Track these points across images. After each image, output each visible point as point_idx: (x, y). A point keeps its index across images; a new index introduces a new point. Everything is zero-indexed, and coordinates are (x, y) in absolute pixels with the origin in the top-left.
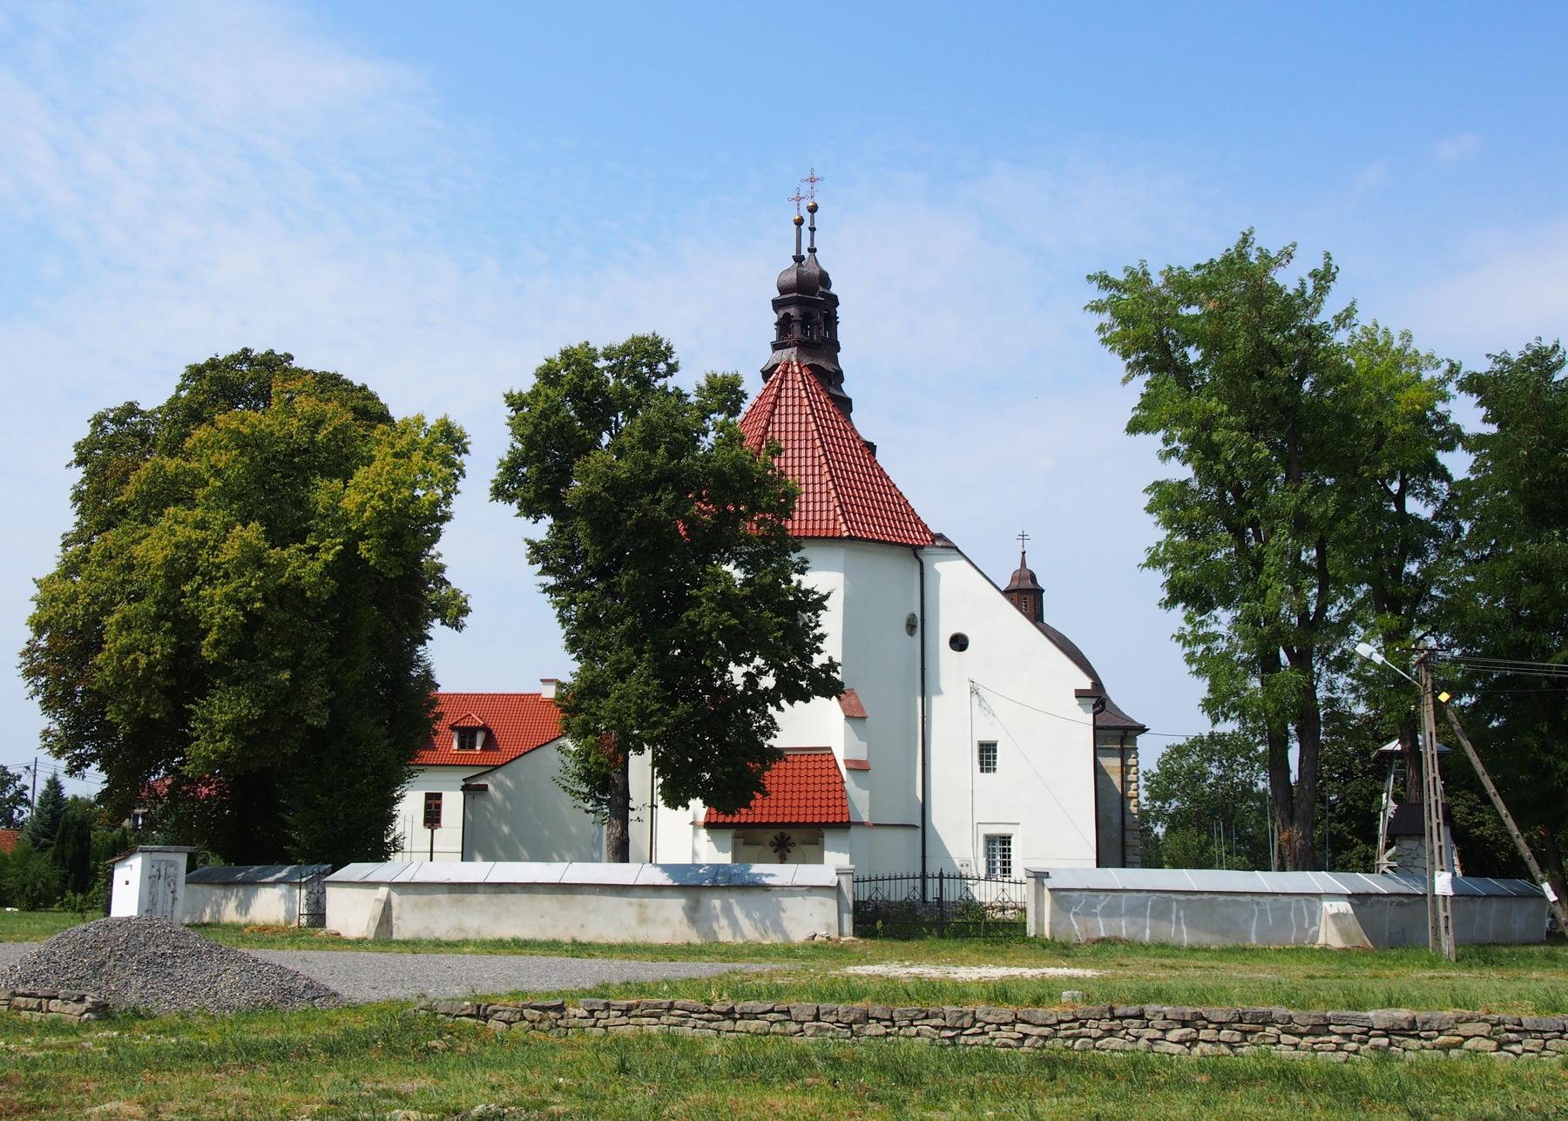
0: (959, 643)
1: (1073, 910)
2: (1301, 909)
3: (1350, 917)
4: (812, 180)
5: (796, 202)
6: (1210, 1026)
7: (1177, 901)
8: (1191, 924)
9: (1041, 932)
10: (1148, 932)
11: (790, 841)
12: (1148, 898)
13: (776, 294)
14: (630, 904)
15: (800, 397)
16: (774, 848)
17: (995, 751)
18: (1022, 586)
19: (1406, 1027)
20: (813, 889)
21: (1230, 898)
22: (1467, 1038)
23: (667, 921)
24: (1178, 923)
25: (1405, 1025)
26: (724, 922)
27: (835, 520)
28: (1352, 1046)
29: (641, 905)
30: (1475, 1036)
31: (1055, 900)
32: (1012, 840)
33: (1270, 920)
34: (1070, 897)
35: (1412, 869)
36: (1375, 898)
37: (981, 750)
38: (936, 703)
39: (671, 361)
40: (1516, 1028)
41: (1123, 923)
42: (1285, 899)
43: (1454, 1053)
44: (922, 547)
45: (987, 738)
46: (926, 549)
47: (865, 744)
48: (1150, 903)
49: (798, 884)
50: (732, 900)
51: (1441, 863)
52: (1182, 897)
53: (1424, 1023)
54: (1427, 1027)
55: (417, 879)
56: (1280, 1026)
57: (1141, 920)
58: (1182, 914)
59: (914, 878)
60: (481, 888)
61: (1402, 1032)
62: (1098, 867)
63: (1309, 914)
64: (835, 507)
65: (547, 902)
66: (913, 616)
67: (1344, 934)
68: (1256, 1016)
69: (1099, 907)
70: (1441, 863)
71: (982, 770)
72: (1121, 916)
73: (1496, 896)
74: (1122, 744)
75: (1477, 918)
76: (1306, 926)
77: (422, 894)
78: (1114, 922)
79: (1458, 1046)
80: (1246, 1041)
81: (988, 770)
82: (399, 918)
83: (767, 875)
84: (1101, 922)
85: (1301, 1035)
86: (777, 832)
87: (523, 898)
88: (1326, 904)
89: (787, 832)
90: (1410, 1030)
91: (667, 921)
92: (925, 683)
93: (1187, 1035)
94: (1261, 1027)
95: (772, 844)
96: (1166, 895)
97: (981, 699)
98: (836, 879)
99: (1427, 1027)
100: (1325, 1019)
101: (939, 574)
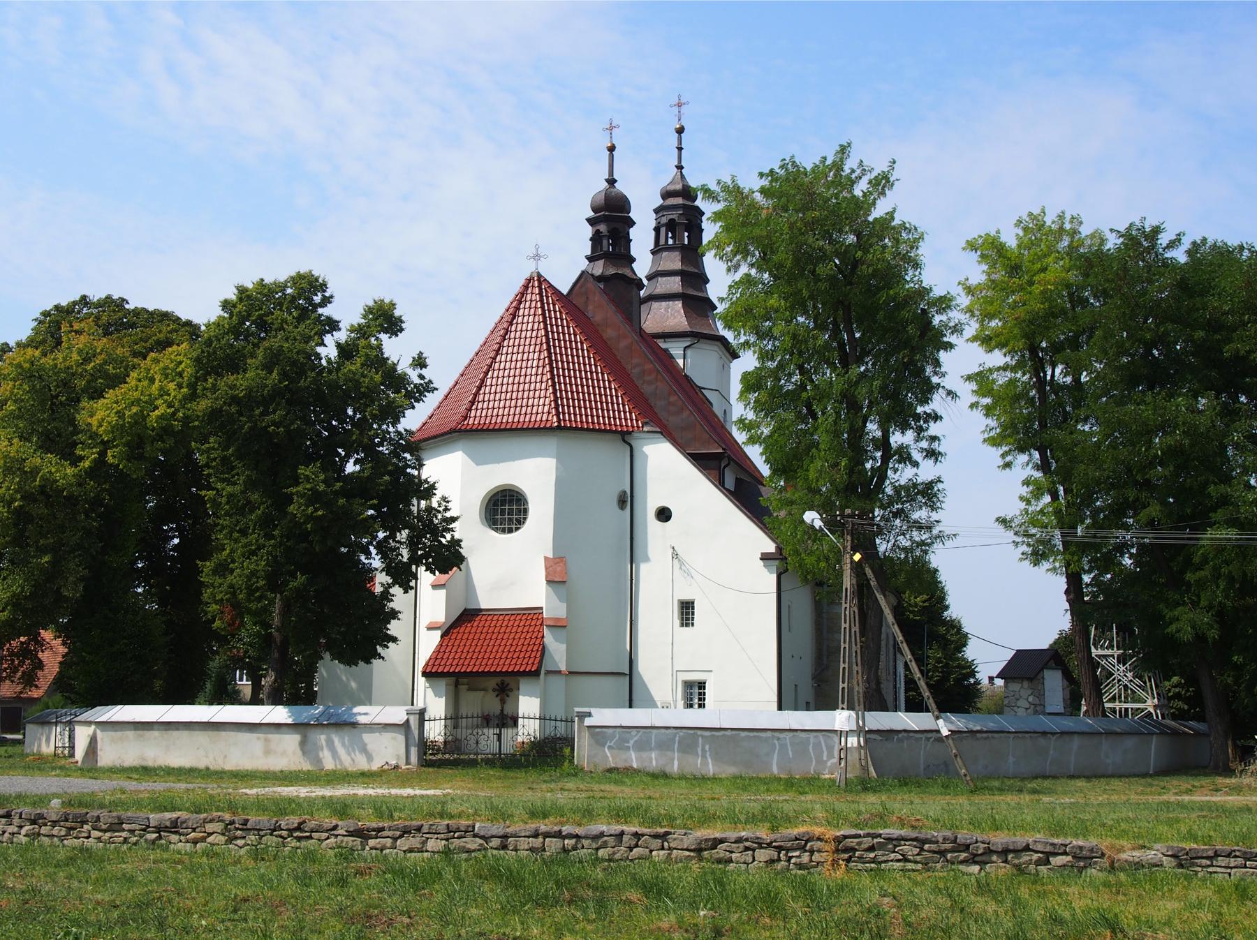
0: (664, 514)
1: (608, 744)
2: (820, 742)
4: (680, 105)
5: (608, 131)
6: (49, 824)
7: (703, 737)
8: (717, 758)
9: (581, 763)
10: (676, 763)
11: (508, 688)
13: (591, 214)
14: (258, 739)
16: (496, 693)
17: (693, 608)
21: (751, 734)
22: (210, 834)
23: (284, 753)
24: (704, 756)
25: (168, 824)
27: (549, 413)
29: (266, 740)
31: (592, 735)
33: (790, 753)
35: (1015, 708)
36: (903, 734)
37: (682, 608)
38: (644, 570)
39: (327, 294)
41: (653, 756)
44: (629, 433)
45: (686, 597)
46: (635, 435)
47: (565, 604)
48: (677, 739)
51: (843, 703)
52: (707, 733)
53: (183, 823)
54: (184, 826)
55: (112, 720)
57: (669, 753)
58: (707, 747)
60: (156, 726)
61: (166, 829)
62: (780, 708)
65: (201, 737)
66: (625, 492)
69: (632, 742)
70: (843, 703)
71: (682, 625)
72: (651, 749)
73: (1075, 733)
75: (1051, 752)
76: (825, 758)
77: (116, 731)
78: (645, 755)
81: (687, 625)
82: (101, 750)
85: (105, 831)
86: (498, 680)
87: (184, 734)
89: (507, 679)
90: (175, 827)
91: (284, 753)
92: (633, 550)
95: (494, 690)
96: (692, 732)
97: (682, 563)
99: (184, 826)
100: (119, 818)
101: (647, 456)
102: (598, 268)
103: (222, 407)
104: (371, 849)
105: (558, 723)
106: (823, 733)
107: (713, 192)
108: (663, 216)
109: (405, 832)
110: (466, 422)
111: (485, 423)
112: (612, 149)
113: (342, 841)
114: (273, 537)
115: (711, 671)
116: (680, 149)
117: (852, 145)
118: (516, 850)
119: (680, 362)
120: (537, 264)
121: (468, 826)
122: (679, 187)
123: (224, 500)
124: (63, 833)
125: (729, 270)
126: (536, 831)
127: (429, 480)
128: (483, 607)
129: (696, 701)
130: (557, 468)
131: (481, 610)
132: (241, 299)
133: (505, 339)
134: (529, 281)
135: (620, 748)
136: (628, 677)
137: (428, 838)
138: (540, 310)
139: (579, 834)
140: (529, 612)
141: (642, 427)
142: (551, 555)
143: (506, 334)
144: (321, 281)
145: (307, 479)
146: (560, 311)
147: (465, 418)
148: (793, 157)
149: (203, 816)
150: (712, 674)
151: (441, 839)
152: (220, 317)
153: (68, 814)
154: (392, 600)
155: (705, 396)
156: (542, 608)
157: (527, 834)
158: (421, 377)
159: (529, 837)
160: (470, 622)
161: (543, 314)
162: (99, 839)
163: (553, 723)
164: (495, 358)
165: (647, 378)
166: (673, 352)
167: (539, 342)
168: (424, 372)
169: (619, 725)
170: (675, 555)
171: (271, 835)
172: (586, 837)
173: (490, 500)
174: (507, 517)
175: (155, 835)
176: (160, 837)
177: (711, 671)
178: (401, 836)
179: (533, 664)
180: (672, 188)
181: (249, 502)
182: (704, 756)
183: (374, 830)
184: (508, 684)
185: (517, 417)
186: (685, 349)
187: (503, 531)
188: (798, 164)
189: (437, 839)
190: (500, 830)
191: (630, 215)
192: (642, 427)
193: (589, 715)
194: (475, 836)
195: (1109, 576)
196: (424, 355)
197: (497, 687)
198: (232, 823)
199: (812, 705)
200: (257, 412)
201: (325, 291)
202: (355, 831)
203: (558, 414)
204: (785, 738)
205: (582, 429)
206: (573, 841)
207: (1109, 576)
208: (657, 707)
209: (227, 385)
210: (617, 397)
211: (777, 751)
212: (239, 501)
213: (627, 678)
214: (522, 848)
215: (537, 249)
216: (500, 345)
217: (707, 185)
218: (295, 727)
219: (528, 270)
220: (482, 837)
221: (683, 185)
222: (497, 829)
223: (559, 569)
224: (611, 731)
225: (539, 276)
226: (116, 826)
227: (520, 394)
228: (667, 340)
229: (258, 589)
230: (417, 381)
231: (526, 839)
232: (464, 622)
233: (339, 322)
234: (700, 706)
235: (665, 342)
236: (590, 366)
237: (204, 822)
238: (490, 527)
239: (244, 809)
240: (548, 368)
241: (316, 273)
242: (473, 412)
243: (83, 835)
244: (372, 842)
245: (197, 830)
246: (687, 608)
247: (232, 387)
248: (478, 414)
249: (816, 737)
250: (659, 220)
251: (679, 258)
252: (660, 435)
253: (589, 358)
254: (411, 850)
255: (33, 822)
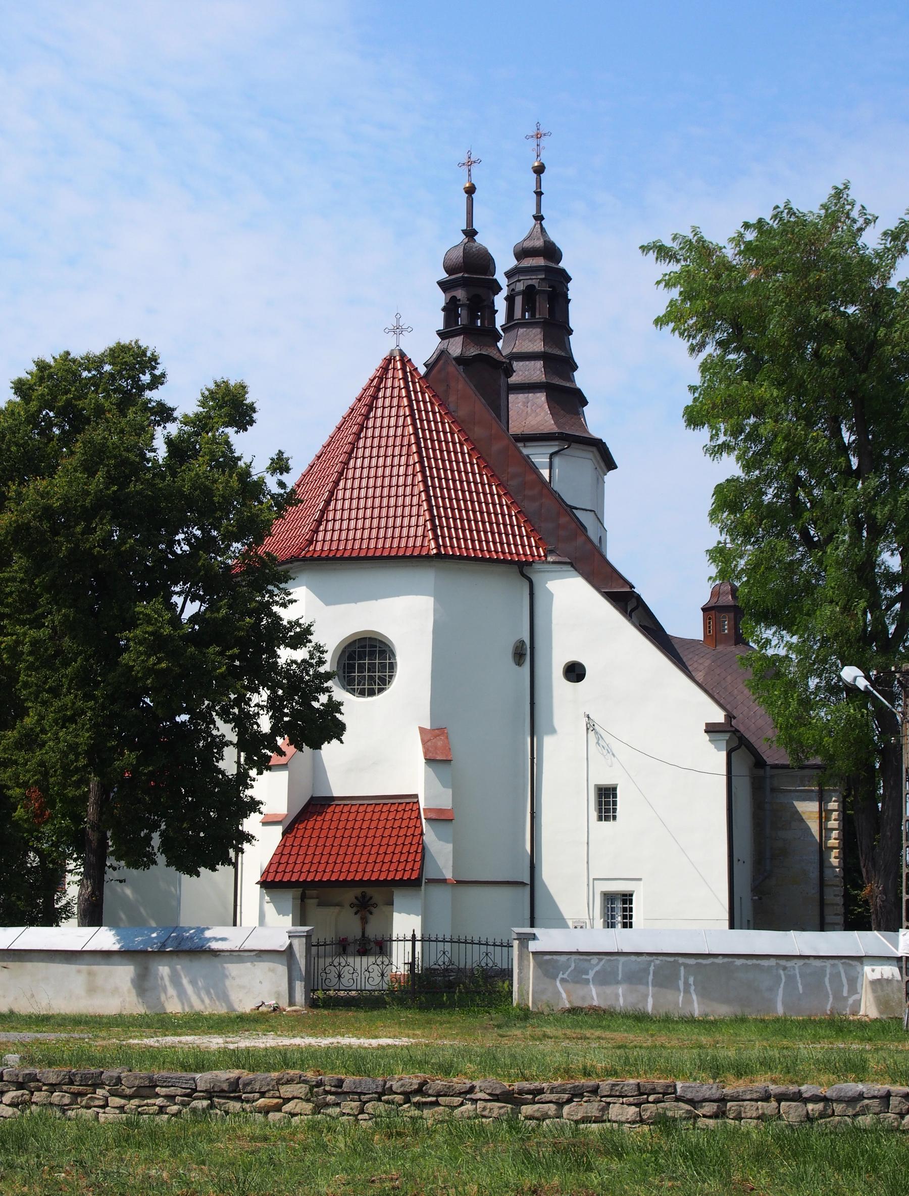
0: (575, 672)
1: (561, 976)
2: (839, 974)
3: (895, 984)
4: (538, 136)
6: (44, 1088)
7: (686, 966)
8: (705, 993)
10: (650, 1001)
11: (372, 902)
12: (650, 962)
13: (444, 275)
14: (79, 971)
15: (400, 397)
16: (355, 909)
17: (615, 796)
18: (720, 603)
19: (226, 1089)
20: (262, 954)
21: (750, 962)
22: (287, 1100)
23: (116, 991)
24: (687, 991)
25: (225, 1086)
26: (171, 991)
27: (424, 536)
28: (175, 1108)
29: (90, 973)
30: (293, 1098)
31: (539, 965)
32: (634, 898)
34: (557, 961)
38: (549, 745)
39: (157, 372)
40: (333, 1089)
41: (620, 991)
42: (817, 963)
43: (273, 1116)
44: (529, 564)
46: (537, 566)
47: (450, 791)
48: (652, 968)
49: (246, 948)
50: (179, 967)
52: (692, 961)
53: (246, 1085)
54: (249, 1089)
56: (107, 1088)
57: (641, 988)
58: (691, 980)
59: (405, 940)
62: (732, 926)
63: (848, 980)
64: (426, 521)
66: (522, 642)
67: (883, 1003)
68: (85, 1078)
74: (820, 785)
76: (845, 994)
78: (609, 990)
79: (278, 1108)
80: (77, 1104)
81: (607, 819)
83: (216, 939)
84: (594, 990)
85: (130, 1097)
86: (358, 891)
88: (867, 969)
89: (370, 891)
91: (116, 991)
93: (18, 1098)
94: (90, 1089)
95: (352, 905)
96: (671, 959)
97: (599, 737)
98: (288, 942)
99: (249, 1089)
100: (151, 1079)
101: (552, 595)
102: (456, 347)
103: (30, 522)
104: (527, 1118)
105: (491, 949)
106: (843, 961)
107: (670, 249)
108: (519, 281)
109: (574, 1095)
110: (312, 548)
111: (337, 549)
112: (470, 191)
113: (484, 1109)
114: (94, 698)
115: (640, 879)
116: (539, 194)
117: (851, 186)
118: (739, 1118)
119: (545, 473)
120: (398, 340)
121: (668, 1086)
122: (539, 243)
123: (26, 648)
124: (66, 1100)
125: (692, 349)
126: (766, 1091)
127: (301, 621)
128: (336, 794)
129: (619, 919)
130: (435, 610)
131: (333, 799)
132: (41, 379)
133: (359, 438)
134: (389, 360)
135: (577, 982)
136: (528, 889)
137: (609, 1103)
138: (405, 399)
139: (828, 1095)
140: (400, 801)
141: (545, 556)
142: (427, 726)
143: (361, 431)
144: (149, 354)
145: (149, 620)
146: (431, 402)
147: (310, 542)
148: (788, 203)
149: (275, 1075)
150: (641, 882)
151: (630, 1105)
152: (10, 402)
153: (74, 1075)
154: (252, 787)
155: (577, 518)
156: (416, 796)
157: (755, 1096)
158: (281, 484)
159: (756, 1100)
160: (320, 814)
161: (410, 406)
162: (121, 1108)
163: (483, 948)
164: (346, 463)
165: (528, 493)
166: (536, 460)
167: (406, 442)
168: (285, 478)
169: (575, 950)
170: (591, 726)
171: (379, 1100)
172: (839, 1100)
173: (343, 652)
174: (366, 674)
175: (205, 1103)
176: (212, 1106)
177: (640, 879)
178: (569, 1101)
179: (412, 870)
180: (529, 244)
181: (59, 652)
182: (687, 991)
183: (529, 1092)
184: (371, 898)
185: (396, 541)
186: (552, 456)
187: (362, 693)
188: (796, 211)
189: (623, 1103)
190: (714, 1091)
191: (495, 277)
192: (545, 556)
193: (534, 937)
194: (678, 1099)
195: (877, 766)
196: (285, 456)
197: (355, 901)
198: (320, 1084)
199: (752, 923)
200: (78, 529)
201: (154, 368)
202: (503, 1093)
203: (436, 538)
204: (794, 968)
205: (468, 558)
206: (820, 1106)
207: (877, 766)
208: (568, 927)
209: (37, 491)
210: (510, 516)
211: (782, 985)
212: (46, 650)
213: (528, 889)
214: (749, 1115)
215: (398, 320)
216: (354, 445)
217: (660, 241)
218: (125, 954)
219: (386, 346)
220: (690, 1102)
221: (545, 241)
222: (708, 1088)
223: (440, 743)
224: (563, 958)
225: (402, 355)
226: (147, 1090)
227: (369, 512)
228: (528, 444)
229: (77, 770)
230: (276, 490)
231: (753, 1103)
232: (312, 814)
233: (173, 410)
234: (625, 925)
235: (525, 446)
236: (474, 474)
237: (278, 1084)
238: (344, 688)
239: (141, 1061)
240: (419, 477)
241: (143, 344)
242: (321, 535)
243: (97, 1103)
244: (527, 1110)
245: (267, 1095)
246: (607, 796)
247: (44, 495)
248: (328, 537)
249: (833, 965)
250: (512, 287)
251: (541, 336)
252: (569, 568)
253: (472, 465)
254: (585, 1120)
255: (20, 1086)
